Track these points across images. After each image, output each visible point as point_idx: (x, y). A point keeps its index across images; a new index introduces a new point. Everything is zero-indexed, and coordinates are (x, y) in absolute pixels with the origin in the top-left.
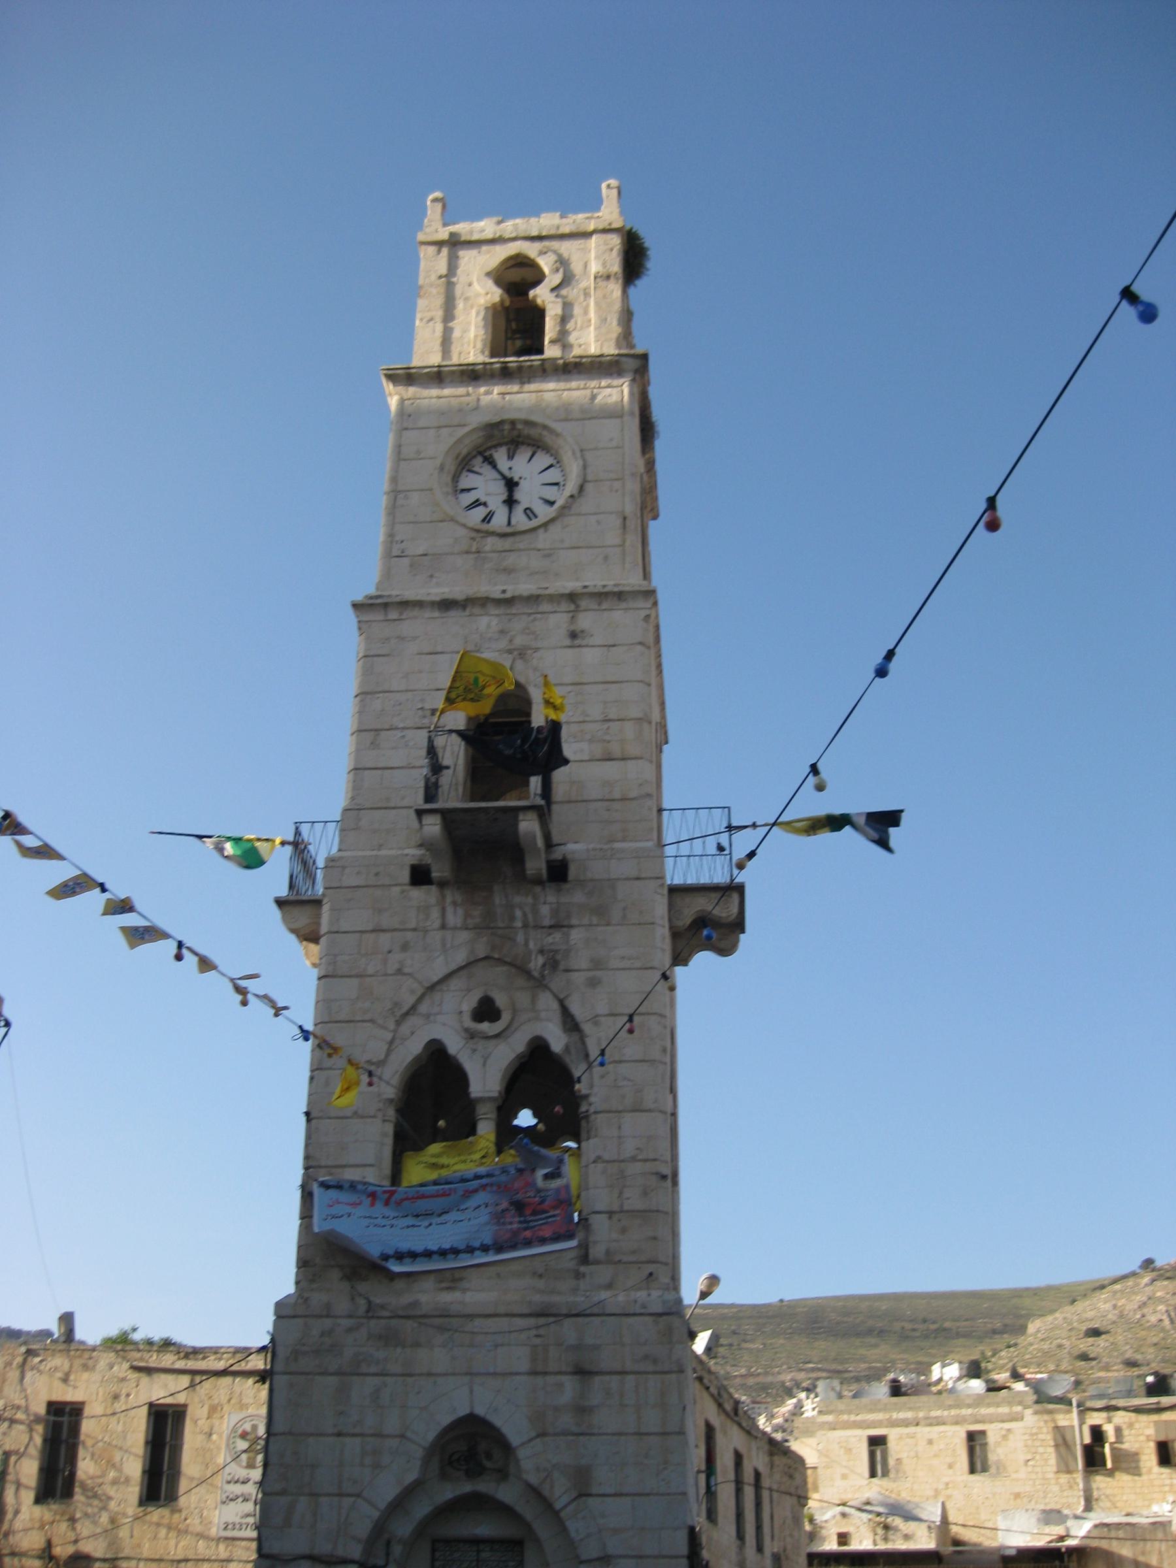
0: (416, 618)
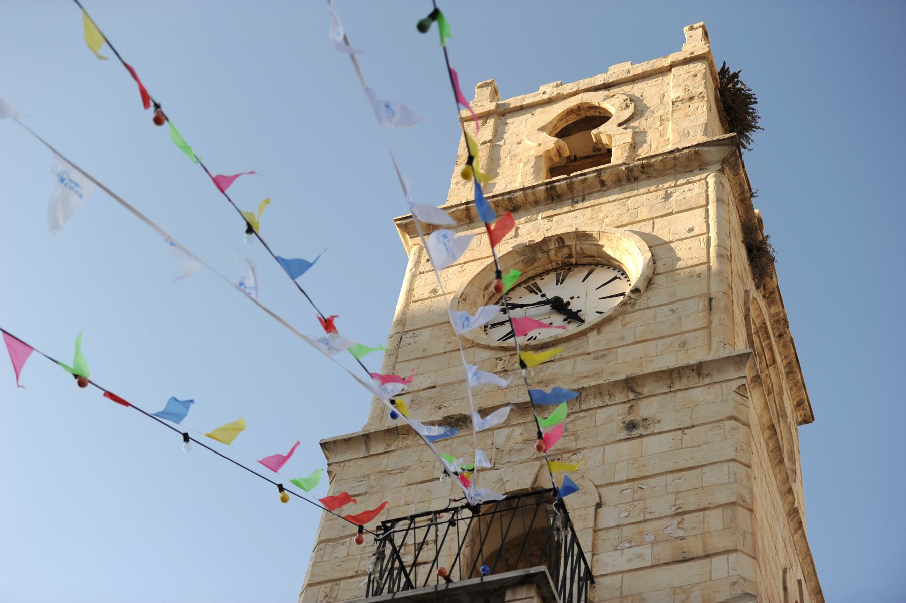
0: (408, 447)
